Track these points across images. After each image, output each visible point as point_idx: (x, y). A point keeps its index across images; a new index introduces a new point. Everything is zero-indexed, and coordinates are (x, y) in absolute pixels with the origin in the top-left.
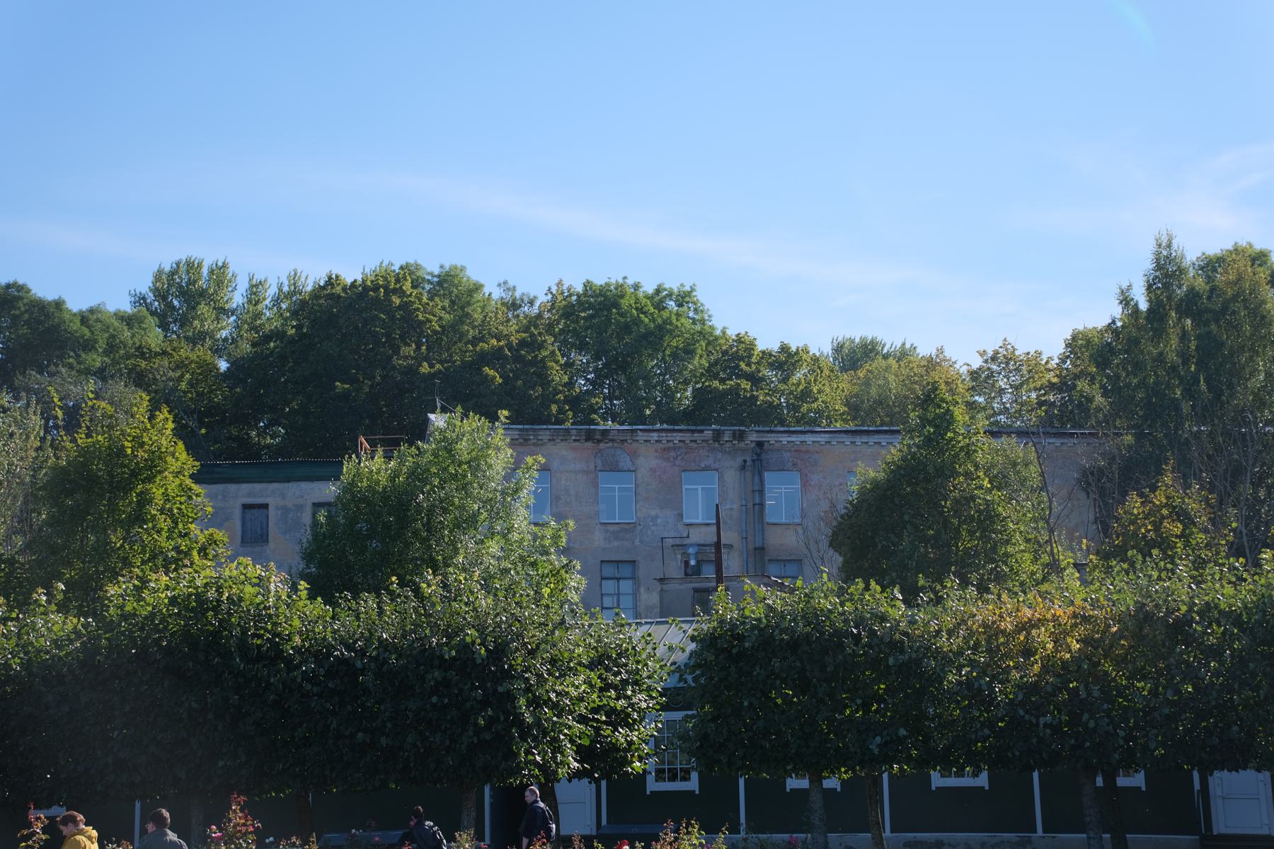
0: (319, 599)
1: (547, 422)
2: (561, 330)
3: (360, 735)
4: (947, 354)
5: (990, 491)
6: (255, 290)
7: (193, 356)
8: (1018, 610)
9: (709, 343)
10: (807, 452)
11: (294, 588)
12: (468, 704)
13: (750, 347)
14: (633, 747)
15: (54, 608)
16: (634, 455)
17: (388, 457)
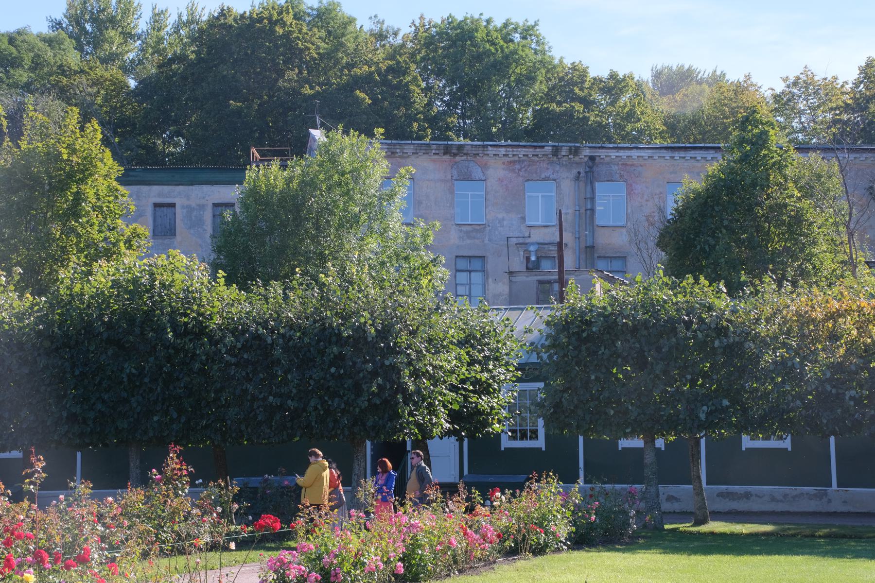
0: (234, 285)
1: (410, 137)
3: (271, 398)
4: (754, 80)
5: (799, 199)
6: (158, 18)
7: (107, 75)
8: (827, 302)
10: (632, 165)
12: (361, 375)
13: (584, 74)
14: (493, 412)
15: (12, 287)
16: (484, 167)
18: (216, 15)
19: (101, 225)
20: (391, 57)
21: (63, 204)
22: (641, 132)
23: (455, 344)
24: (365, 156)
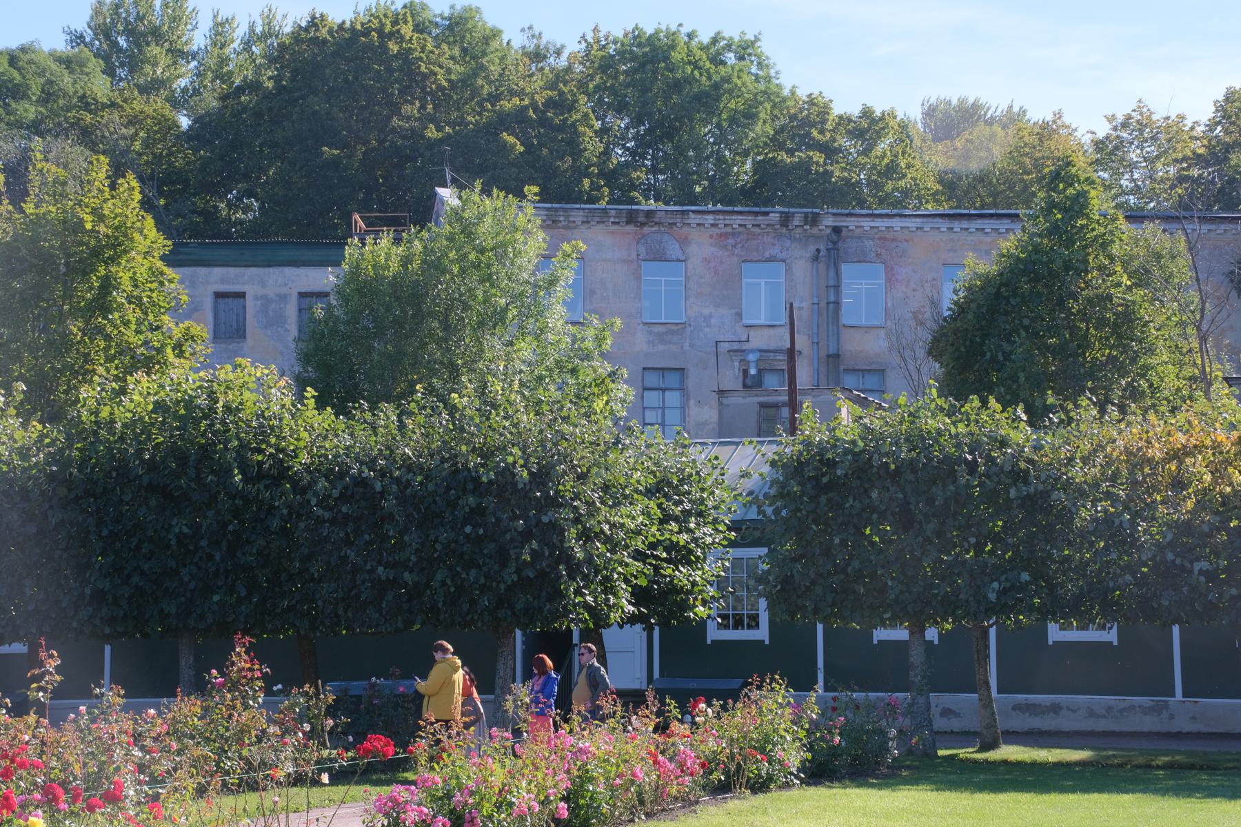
0: (329, 409)
2: (596, 87)
3: (381, 569)
4: (1067, 119)
5: (1129, 288)
6: (220, 29)
7: (149, 110)
8: (1169, 434)
9: (774, 106)
10: (894, 240)
11: (301, 398)
12: (508, 536)
13: (825, 110)
14: (696, 589)
16: (684, 242)
17: (397, 241)
18: (304, 24)
19: (139, 323)
20: (552, 86)
21: (86, 292)
22: (906, 193)
23: (641, 493)
24: (515, 226)
